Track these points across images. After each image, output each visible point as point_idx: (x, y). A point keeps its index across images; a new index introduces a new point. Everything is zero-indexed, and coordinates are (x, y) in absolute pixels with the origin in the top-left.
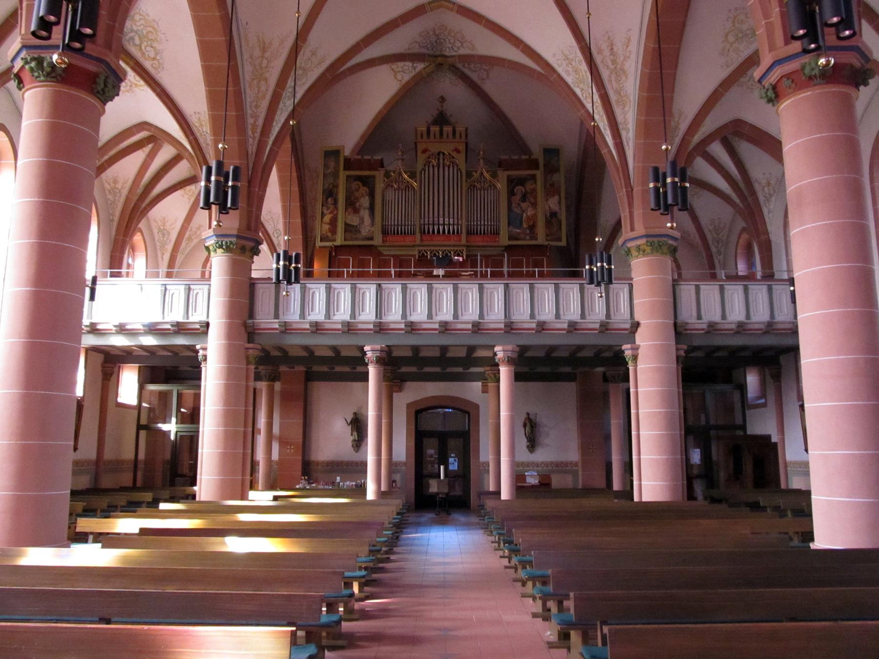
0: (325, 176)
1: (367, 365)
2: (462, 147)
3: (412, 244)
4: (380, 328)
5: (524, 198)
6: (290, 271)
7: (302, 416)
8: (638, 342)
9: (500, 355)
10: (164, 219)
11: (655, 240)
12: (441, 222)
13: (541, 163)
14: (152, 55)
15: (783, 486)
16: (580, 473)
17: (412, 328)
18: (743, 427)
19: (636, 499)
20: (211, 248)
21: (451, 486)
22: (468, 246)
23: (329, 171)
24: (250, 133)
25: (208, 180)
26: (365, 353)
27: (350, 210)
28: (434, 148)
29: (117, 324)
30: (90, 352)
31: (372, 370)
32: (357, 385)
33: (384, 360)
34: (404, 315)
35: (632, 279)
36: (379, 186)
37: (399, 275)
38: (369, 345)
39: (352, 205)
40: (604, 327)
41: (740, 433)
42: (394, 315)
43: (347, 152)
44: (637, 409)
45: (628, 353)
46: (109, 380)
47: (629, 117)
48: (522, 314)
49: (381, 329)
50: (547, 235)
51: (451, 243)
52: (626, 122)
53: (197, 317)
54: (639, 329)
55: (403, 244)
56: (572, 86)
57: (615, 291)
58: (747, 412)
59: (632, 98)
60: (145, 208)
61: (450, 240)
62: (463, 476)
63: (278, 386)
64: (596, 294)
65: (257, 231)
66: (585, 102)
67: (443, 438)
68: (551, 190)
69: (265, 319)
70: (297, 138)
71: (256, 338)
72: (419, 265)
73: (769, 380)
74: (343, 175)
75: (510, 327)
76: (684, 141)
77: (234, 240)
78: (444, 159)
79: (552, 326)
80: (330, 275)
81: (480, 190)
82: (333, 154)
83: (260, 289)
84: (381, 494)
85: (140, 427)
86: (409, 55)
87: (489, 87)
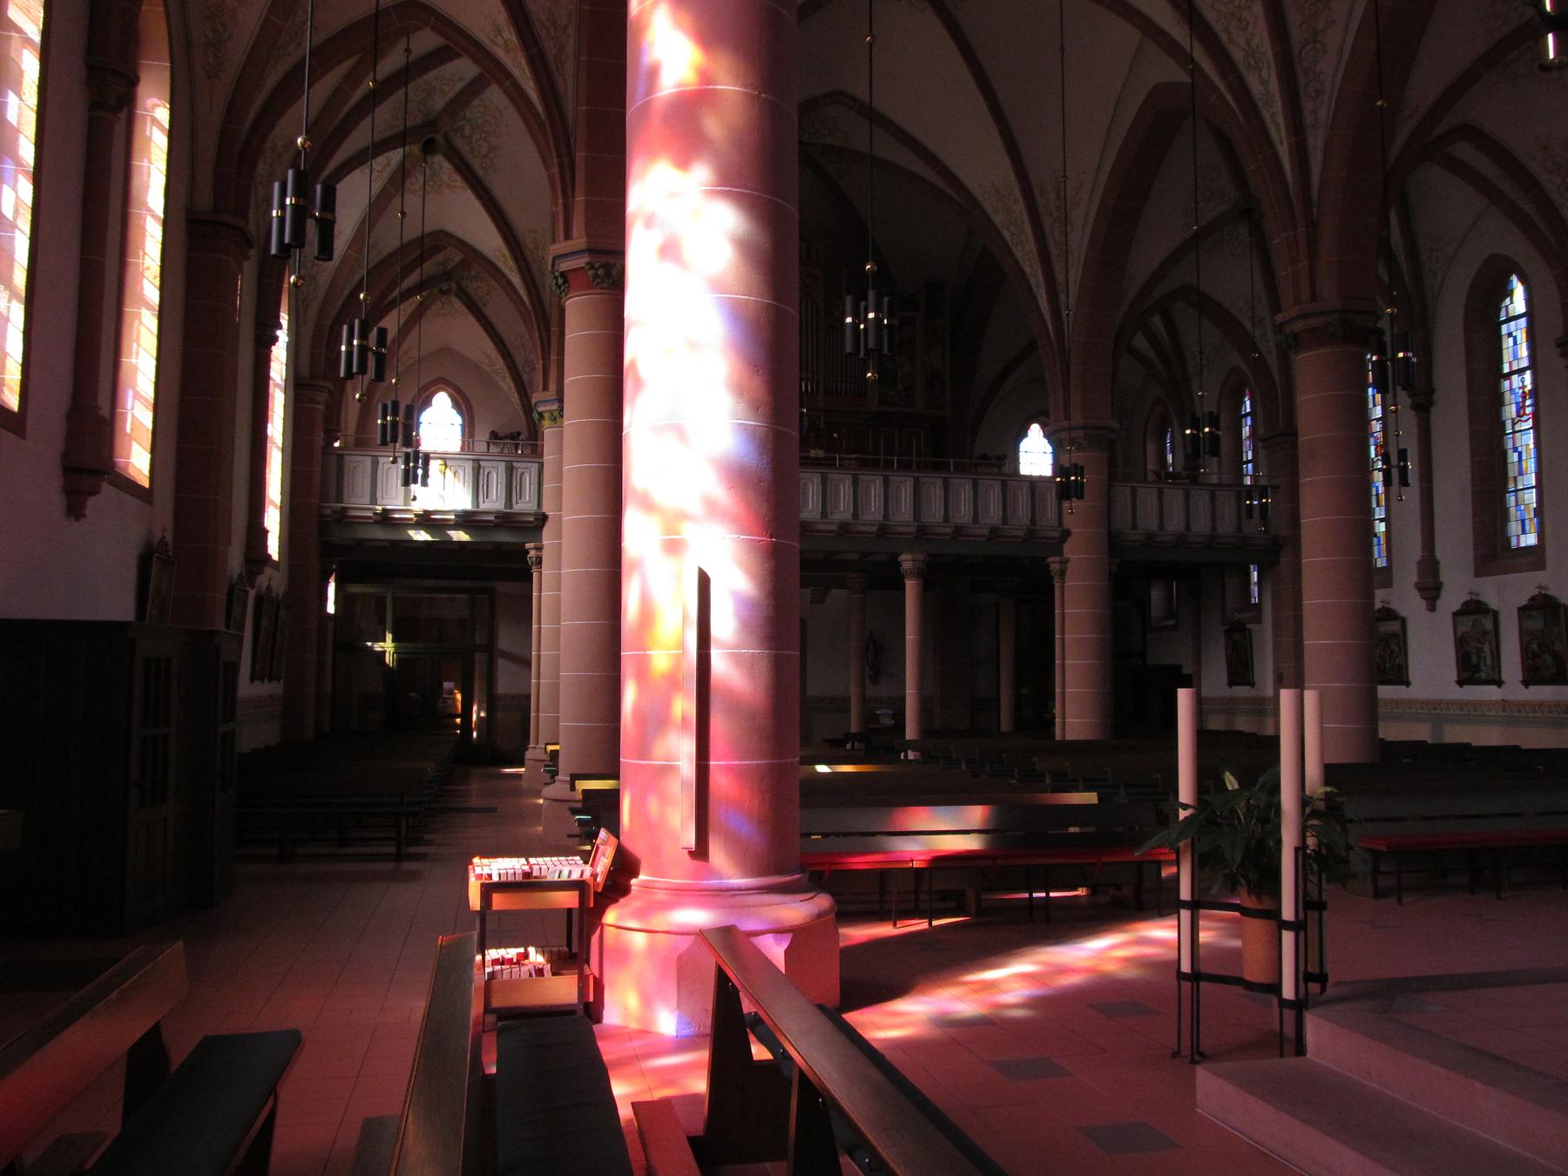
14: (484, 151)
40: (1031, 534)
45: (1054, 567)
47: (1073, 277)
48: (934, 512)
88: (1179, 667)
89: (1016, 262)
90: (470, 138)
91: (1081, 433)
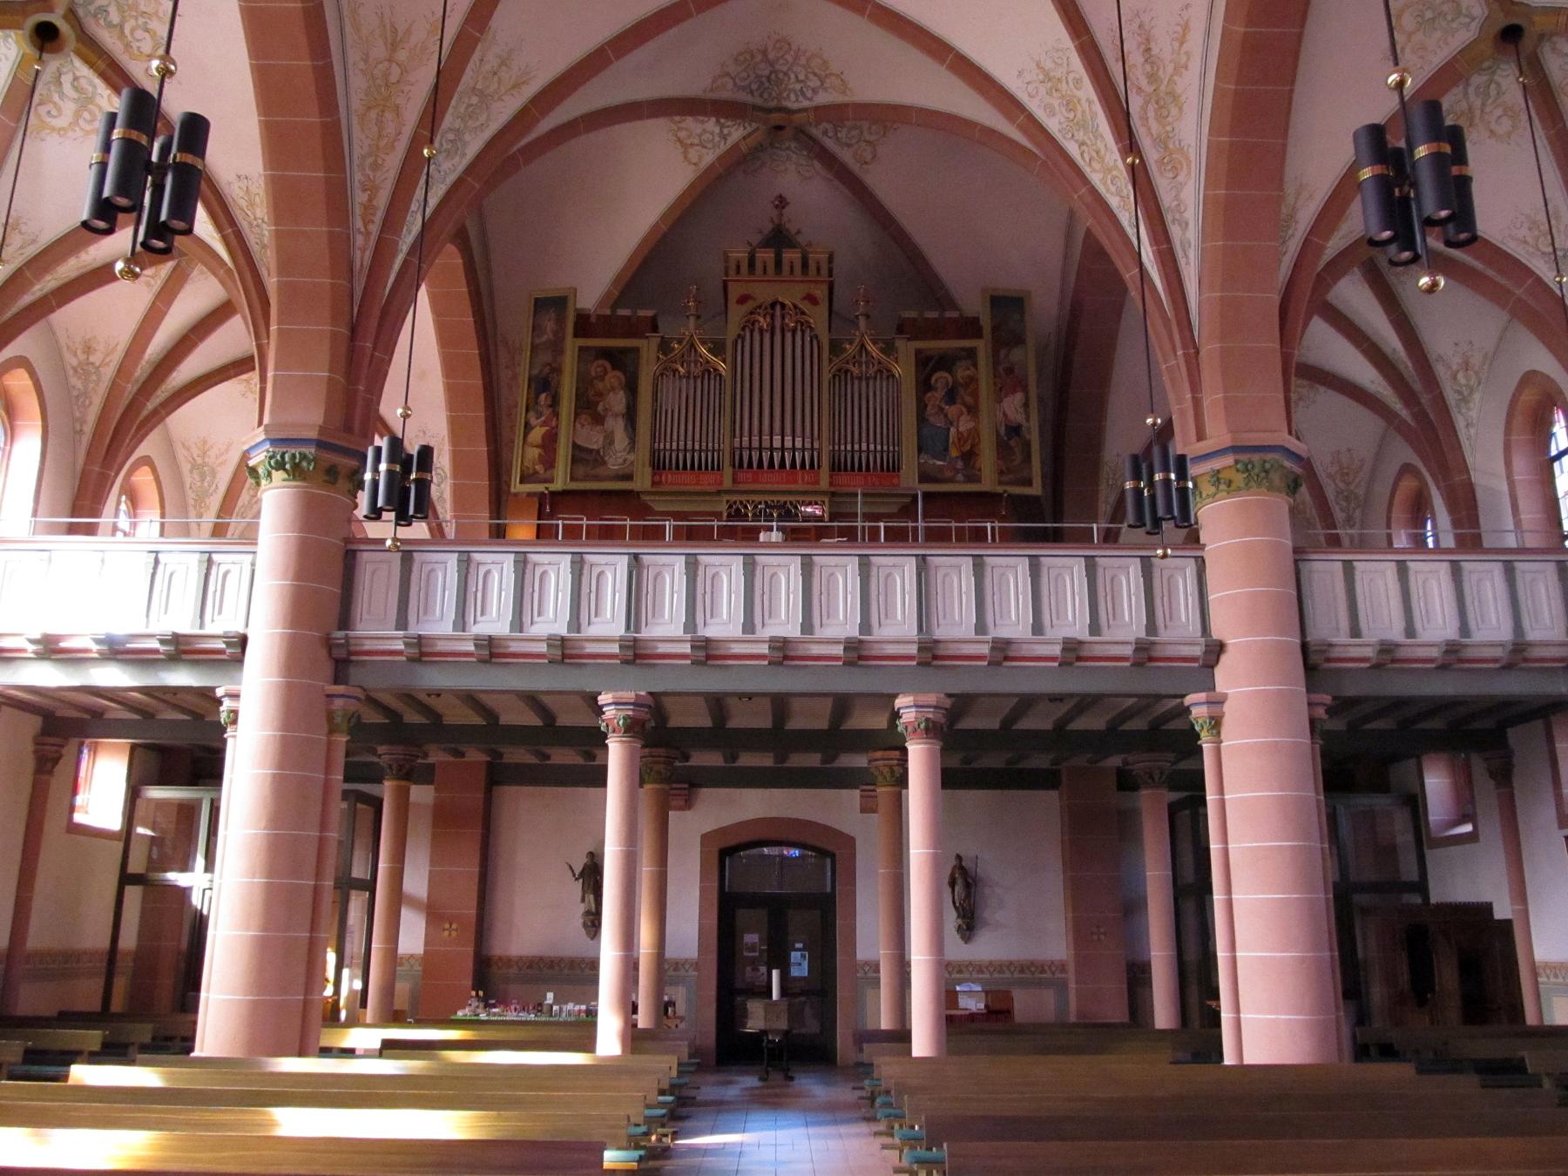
0: (534, 348)
2: (821, 292)
3: (713, 489)
4: (636, 653)
5: (951, 396)
7: (476, 860)
8: (1221, 686)
9: (908, 716)
10: (205, 442)
11: (1256, 458)
13: (986, 323)
15: (1531, 1019)
16: (1072, 985)
17: (707, 652)
18: (1421, 887)
19: (1229, 1059)
20: (261, 471)
21: (795, 1015)
22: (833, 494)
23: (545, 338)
24: (359, 224)
26: (599, 711)
28: (764, 293)
29: (38, 636)
30: (139, 750)
31: (616, 754)
32: (593, 791)
34: (690, 624)
38: (609, 690)
40: (1145, 654)
41: (1417, 899)
42: (666, 624)
45: (1199, 713)
46: (51, 772)
47: (1187, 197)
48: (956, 622)
49: (637, 656)
50: (1001, 473)
51: (800, 487)
53: (222, 623)
54: (1224, 658)
55: (698, 488)
57: (1166, 574)
58: (1429, 853)
60: (155, 412)
61: (795, 482)
62: (820, 992)
63: (421, 794)
66: (1087, 170)
67: (777, 911)
68: (1009, 380)
69: (376, 629)
71: (355, 674)
72: (733, 521)
73: (1485, 788)
74: (571, 345)
75: (931, 654)
76: (1310, 247)
77: (310, 451)
78: (783, 318)
79: (1025, 651)
81: (860, 379)
84: (634, 1038)
85: (126, 879)
86: (715, 102)
87: (880, 181)
88: (1488, 908)
89: (1093, 191)
90: (121, 27)
91: (1229, 460)
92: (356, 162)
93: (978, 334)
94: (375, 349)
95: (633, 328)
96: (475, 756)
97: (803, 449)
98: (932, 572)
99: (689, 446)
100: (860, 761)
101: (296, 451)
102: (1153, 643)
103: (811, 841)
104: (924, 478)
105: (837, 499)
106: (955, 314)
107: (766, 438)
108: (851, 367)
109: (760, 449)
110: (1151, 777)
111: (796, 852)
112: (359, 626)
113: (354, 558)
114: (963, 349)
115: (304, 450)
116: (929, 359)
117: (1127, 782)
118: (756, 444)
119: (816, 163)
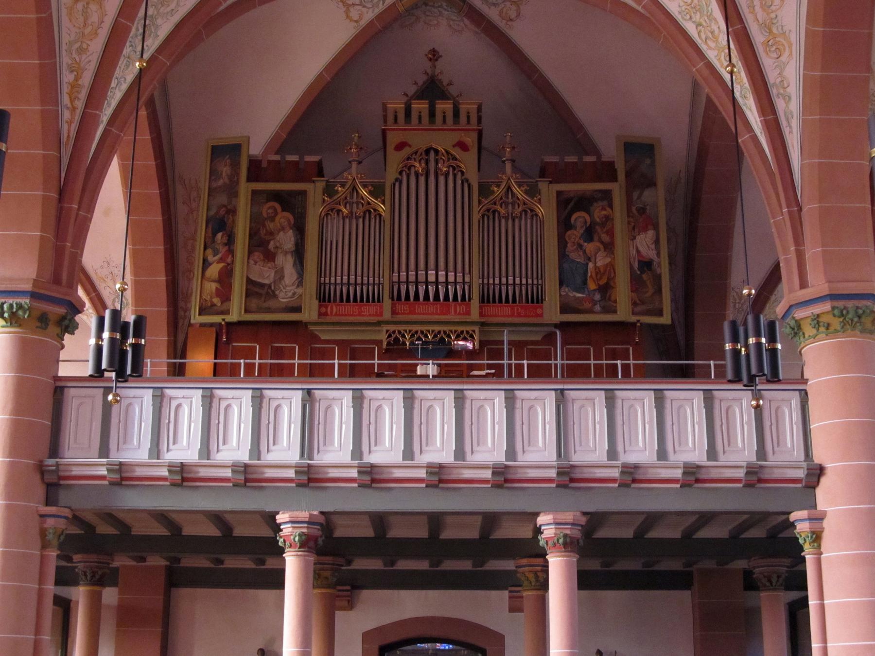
0: (211, 192)
1: (282, 551)
2: (470, 139)
4: (310, 478)
5: (589, 234)
6: (124, 353)
8: (821, 505)
9: (549, 532)
11: (850, 304)
12: (432, 278)
17: (372, 477)
22: (483, 324)
24: (66, 100)
25: (99, 337)
26: (277, 528)
27: (257, 255)
28: (419, 141)
31: (293, 565)
32: (266, 595)
33: (315, 539)
34: (357, 452)
35: (805, 382)
36: (314, 211)
37: (352, 373)
38: (287, 509)
39: (261, 245)
40: (755, 477)
42: (336, 453)
43: (256, 148)
44: (824, 640)
45: (802, 528)
48: (591, 450)
50: (635, 304)
51: (451, 317)
52: (783, 85)
54: (823, 480)
56: (679, 18)
59: (793, 38)
61: (448, 313)
63: (110, 595)
64: (738, 405)
65: (72, 287)
66: (703, 47)
68: (641, 220)
69: (81, 457)
70: (162, 123)
71: (64, 497)
72: (389, 359)
74: (245, 189)
75: (569, 478)
77: (25, 301)
78: (437, 162)
79: (652, 474)
80: (217, 371)
81: (507, 219)
82: (227, 152)
83: (73, 395)
91: (826, 306)
92: (64, 47)
93: (612, 177)
94: (79, 209)
95: (300, 173)
96: (157, 561)
97: (455, 283)
98: (570, 405)
99: (352, 280)
100: (509, 565)
101: (14, 301)
102: (761, 467)
103: (461, 638)
104: (564, 309)
105: (486, 328)
106: (591, 159)
107: (422, 273)
108: (498, 208)
109: (417, 283)
110: (770, 581)
111: (447, 647)
112: (67, 454)
113: (62, 393)
114: (600, 191)
115: (18, 301)
116: (568, 201)
117: (750, 583)
118: (412, 278)
119: (465, 20)
